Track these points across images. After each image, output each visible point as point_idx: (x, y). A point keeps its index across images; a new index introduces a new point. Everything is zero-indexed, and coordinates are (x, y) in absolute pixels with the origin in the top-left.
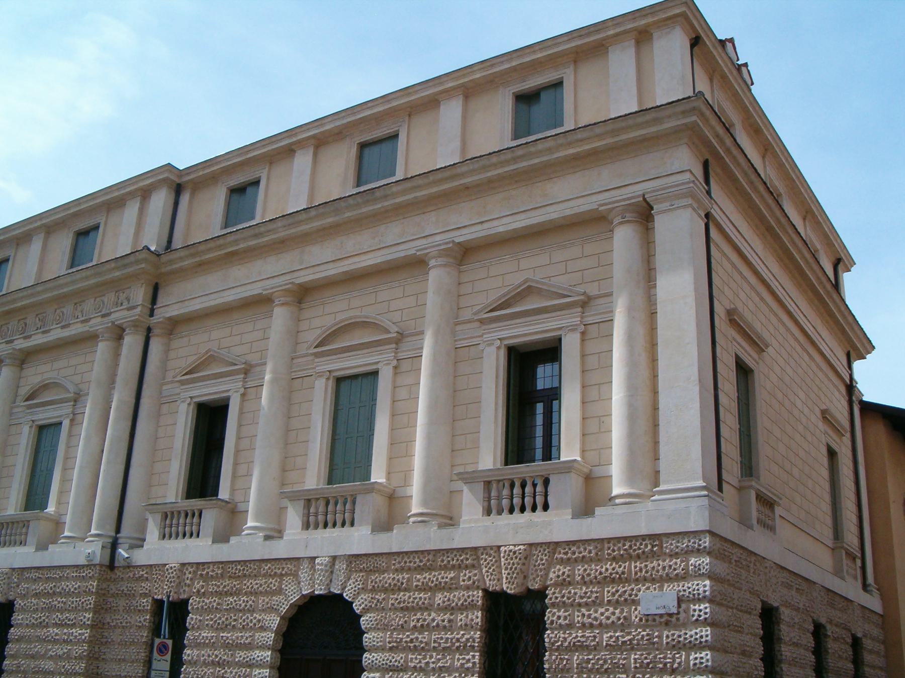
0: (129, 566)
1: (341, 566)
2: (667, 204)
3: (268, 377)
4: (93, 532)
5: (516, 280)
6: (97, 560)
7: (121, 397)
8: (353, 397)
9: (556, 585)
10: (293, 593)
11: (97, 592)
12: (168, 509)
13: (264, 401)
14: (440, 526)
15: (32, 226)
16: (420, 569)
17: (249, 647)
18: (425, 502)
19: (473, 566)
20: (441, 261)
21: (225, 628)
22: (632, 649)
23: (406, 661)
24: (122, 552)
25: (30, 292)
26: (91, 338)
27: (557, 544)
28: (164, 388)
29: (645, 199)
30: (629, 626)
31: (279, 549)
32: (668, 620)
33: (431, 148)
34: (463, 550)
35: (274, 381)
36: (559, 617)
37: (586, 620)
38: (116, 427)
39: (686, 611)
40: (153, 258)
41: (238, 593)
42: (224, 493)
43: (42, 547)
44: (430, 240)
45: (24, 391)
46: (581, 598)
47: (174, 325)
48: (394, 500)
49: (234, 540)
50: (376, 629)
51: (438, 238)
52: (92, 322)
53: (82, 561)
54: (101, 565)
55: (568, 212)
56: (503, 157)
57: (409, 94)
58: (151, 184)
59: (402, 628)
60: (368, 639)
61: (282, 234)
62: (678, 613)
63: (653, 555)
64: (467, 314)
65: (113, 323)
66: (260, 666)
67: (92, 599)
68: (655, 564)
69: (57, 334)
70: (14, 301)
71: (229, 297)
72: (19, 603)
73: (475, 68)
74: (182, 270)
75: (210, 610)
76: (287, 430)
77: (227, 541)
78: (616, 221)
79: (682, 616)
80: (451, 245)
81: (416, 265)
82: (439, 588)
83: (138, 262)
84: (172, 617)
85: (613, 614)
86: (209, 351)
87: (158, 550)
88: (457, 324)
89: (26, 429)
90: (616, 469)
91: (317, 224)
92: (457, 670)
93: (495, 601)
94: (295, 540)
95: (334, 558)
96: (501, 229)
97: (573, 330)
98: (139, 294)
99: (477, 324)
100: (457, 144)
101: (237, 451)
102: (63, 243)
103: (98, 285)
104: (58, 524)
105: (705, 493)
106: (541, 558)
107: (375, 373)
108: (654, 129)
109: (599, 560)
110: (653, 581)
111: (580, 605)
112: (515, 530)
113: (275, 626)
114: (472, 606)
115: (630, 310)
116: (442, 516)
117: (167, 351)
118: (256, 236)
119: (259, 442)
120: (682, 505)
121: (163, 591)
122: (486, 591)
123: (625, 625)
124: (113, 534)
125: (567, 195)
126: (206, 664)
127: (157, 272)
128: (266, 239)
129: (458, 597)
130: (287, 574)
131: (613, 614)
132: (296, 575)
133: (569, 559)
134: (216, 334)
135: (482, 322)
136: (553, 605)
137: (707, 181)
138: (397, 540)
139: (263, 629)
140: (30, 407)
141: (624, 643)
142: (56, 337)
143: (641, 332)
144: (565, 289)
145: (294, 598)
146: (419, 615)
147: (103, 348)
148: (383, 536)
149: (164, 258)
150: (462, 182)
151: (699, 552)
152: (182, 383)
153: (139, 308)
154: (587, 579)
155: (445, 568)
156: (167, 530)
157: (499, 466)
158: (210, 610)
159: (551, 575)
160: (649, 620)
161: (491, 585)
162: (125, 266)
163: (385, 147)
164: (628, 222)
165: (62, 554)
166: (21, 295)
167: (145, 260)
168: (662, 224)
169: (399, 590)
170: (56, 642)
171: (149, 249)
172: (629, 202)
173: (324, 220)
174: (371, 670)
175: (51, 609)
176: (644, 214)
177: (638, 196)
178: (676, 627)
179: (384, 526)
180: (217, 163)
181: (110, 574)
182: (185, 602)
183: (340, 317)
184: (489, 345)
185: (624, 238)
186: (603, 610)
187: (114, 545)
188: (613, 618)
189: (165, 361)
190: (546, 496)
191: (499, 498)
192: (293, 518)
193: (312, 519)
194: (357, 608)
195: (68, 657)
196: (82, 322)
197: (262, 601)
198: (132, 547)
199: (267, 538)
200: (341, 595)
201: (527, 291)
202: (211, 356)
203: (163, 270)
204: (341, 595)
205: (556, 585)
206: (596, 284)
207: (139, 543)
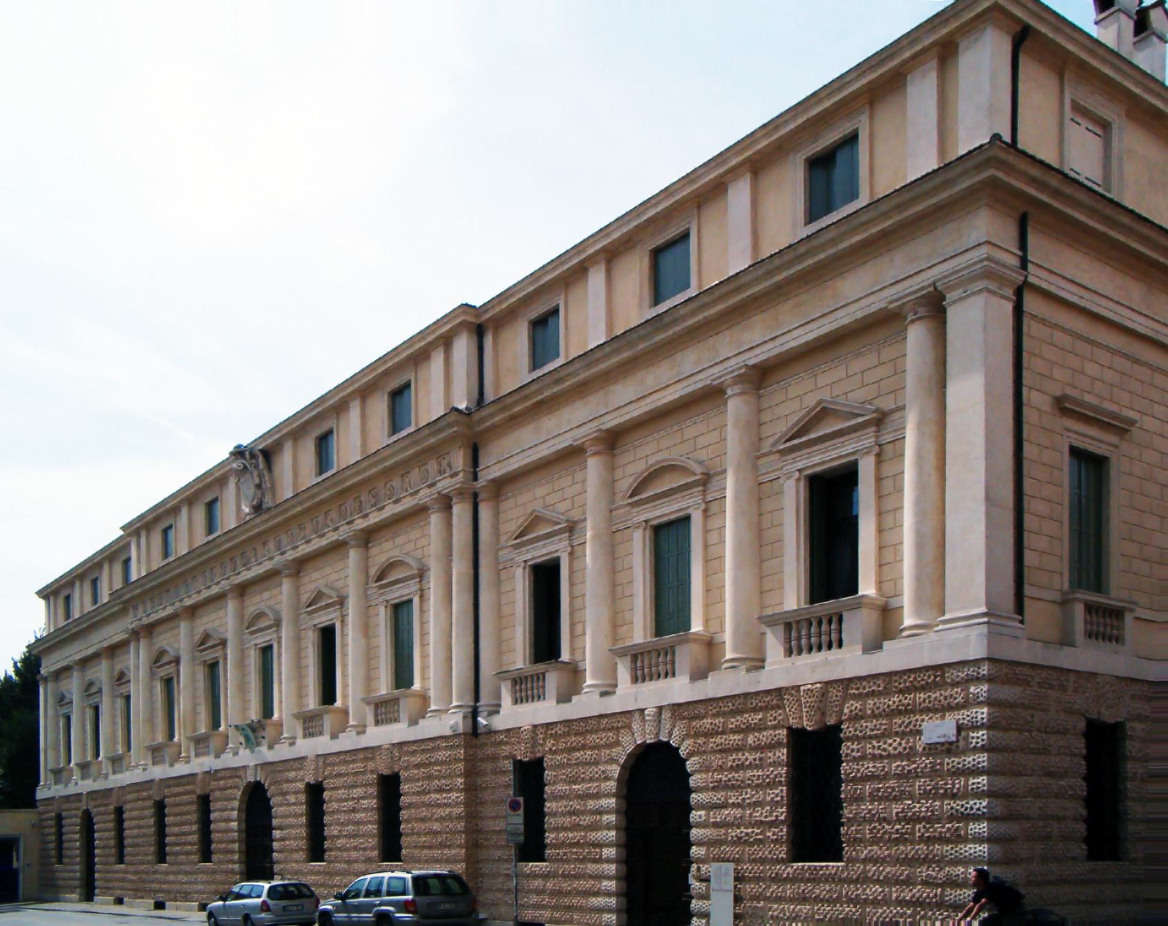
0: (490, 732)
1: (666, 715)
2: (960, 291)
3: (589, 534)
4: (455, 703)
5: (811, 401)
6: (461, 730)
7: (460, 567)
8: (669, 540)
9: (850, 719)
10: (629, 743)
11: (465, 759)
12: (515, 675)
13: (588, 559)
14: (748, 670)
15: (344, 393)
16: (734, 713)
17: (597, 796)
18: (735, 648)
19: (778, 707)
20: (737, 389)
21: (574, 781)
22: (917, 776)
23: (726, 799)
24: (482, 720)
25: (355, 470)
26: (420, 512)
27: (850, 680)
28: (501, 553)
29: (935, 288)
30: (915, 755)
31: (614, 705)
32: (948, 748)
33: (722, 251)
34: (768, 692)
35: (595, 537)
36: (853, 750)
37: (877, 752)
38: (461, 601)
39: (966, 738)
40: (462, 418)
41: (583, 747)
42: (565, 656)
43: (413, 722)
44: (726, 365)
45: (373, 571)
46: (872, 730)
47: (501, 486)
48: (711, 645)
49: (575, 699)
50: (699, 771)
51: (732, 362)
52: (422, 493)
53: (448, 732)
54: (464, 734)
55: (859, 315)
56: (786, 258)
57: (672, 195)
58: (450, 330)
59: (721, 769)
60: (693, 781)
61: (582, 376)
62: (958, 741)
63: (935, 686)
64: (766, 447)
65: (439, 493)
66: (607, 812)
67: (461, 766)
68: (938, 694)
69: (391, 510)
70: (345, 480)
71: (545, 451)
72: (403, 774)
73: (759, 135)
74: (494, 427)
75: (561, 766)
76: (614, 585)
77: (569, 700)
78: (910, 317)
79: (961, 744)
80: (743, 371)
81: (712, 395)
82: (749, 729)
83: (450, 425)
84: (530, 777)
85: (900, 744)
86: (534, 511)
87: (514, 715)
88: (758, 458)
89: (382, 610)
90: (907, 600)
91: (615, 360)
92: (768, 804)
93: (797, 737)
94: (631, 695)
95: (660, 708)
96: (793, 344)
97: (867, 452)
98: (459, 459)
99: (777, 456)
100: (747, 240)
101: (572, 613)
102: (379, 407)
103: (417, 454)
104: (424, 698)
105: (986, 619)
106: (834, 693)
107: (687, 519)
108: (944, 195)
109: (886, 693)
110: (935, 711)
111: (871, 737)
112: (813, 669)
113: (616, 776)
114: (778, 744)
115: (920, 425)
116: (752, 659)
117: (497, 514)
118: (557, 382)
119: (589, 601)
120: (962, 634)
121: (522, 754)
122: (790, 729)
123: (910, 755)
124: (472, 703)
125: (859, 292)
126: (563, 814)
127: (472, 430)
128: (568, 383)
129: (765, 736)
130: (622, 727)
131: (900, 744)
132: (629, 727)
133: (860, 694)
134: (540, 492)
135: (782, 453)
136: (848, 739)
137: (1023, 245)
138: (719, 685)
139: (607, 779)
140: (381, 587)
141: (909, 771)
142: (390, 513)
143: (931, 447)
144: (857, 408)
145: (630, 749)
146: (734, 756)
147: (435, 519)
148: (700, 683)
149: (476, 417)
150: (749, 293)
151: (978, 679)
152: (516, 547)
153: (461, 475)
154: (877, 712)
155: (755, 710)
156: (639, 673)
157: (803, 606)
158: (561, 766)
159: (846, 711)
160: (932, 749)
161: (793, 722)
162: (439, 431)
163: (678, 249)
164: (919, 319)
165: (431, 727)
166: (349, 473)
167: (456, 423)
168: (955, 316)
169: (717, 733)
170: (439, 806)
171: (457, 410)
172: (918, 295)
173: (630, 352)
174: (698, 809)
175: (430, 777)
176: (934, 307)
177: (929, 286)
178: (957, 755)
179: (699, 674)
180: (512, 295)
181: (475, 741)
182: (541, 760)
183: (651, 461)
184: (789, 478)
185: (917, 336)
186: (890, 741)
187: (475, 713)
188: (900, 749)
189: (496, 527)
190: (840, 632)
191: (799, 639)
192: (624, 673)
193: (639, 673)
194: (683, 753)
195: (449, 818)
196: (412, 495)
197: (605, 752)
198: (491, 714)
199: (603, 694)
200: (668, 743)
201: (822, 413)
202: (537, 517)
203: (478, 429)
204: (668, 743)
205: (850, 719)
206: (892, 395)
207: (495, 710)
